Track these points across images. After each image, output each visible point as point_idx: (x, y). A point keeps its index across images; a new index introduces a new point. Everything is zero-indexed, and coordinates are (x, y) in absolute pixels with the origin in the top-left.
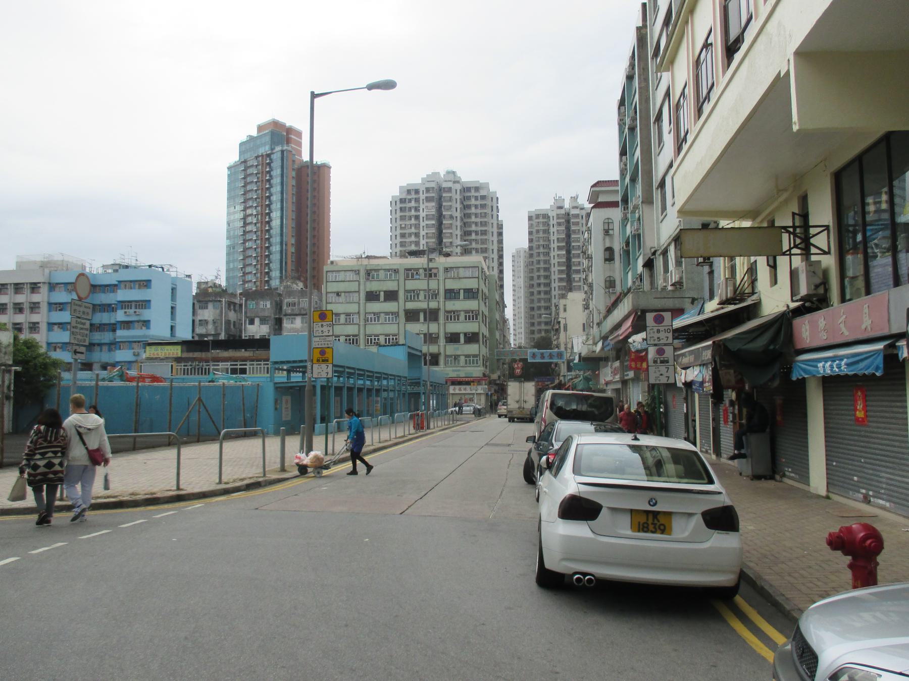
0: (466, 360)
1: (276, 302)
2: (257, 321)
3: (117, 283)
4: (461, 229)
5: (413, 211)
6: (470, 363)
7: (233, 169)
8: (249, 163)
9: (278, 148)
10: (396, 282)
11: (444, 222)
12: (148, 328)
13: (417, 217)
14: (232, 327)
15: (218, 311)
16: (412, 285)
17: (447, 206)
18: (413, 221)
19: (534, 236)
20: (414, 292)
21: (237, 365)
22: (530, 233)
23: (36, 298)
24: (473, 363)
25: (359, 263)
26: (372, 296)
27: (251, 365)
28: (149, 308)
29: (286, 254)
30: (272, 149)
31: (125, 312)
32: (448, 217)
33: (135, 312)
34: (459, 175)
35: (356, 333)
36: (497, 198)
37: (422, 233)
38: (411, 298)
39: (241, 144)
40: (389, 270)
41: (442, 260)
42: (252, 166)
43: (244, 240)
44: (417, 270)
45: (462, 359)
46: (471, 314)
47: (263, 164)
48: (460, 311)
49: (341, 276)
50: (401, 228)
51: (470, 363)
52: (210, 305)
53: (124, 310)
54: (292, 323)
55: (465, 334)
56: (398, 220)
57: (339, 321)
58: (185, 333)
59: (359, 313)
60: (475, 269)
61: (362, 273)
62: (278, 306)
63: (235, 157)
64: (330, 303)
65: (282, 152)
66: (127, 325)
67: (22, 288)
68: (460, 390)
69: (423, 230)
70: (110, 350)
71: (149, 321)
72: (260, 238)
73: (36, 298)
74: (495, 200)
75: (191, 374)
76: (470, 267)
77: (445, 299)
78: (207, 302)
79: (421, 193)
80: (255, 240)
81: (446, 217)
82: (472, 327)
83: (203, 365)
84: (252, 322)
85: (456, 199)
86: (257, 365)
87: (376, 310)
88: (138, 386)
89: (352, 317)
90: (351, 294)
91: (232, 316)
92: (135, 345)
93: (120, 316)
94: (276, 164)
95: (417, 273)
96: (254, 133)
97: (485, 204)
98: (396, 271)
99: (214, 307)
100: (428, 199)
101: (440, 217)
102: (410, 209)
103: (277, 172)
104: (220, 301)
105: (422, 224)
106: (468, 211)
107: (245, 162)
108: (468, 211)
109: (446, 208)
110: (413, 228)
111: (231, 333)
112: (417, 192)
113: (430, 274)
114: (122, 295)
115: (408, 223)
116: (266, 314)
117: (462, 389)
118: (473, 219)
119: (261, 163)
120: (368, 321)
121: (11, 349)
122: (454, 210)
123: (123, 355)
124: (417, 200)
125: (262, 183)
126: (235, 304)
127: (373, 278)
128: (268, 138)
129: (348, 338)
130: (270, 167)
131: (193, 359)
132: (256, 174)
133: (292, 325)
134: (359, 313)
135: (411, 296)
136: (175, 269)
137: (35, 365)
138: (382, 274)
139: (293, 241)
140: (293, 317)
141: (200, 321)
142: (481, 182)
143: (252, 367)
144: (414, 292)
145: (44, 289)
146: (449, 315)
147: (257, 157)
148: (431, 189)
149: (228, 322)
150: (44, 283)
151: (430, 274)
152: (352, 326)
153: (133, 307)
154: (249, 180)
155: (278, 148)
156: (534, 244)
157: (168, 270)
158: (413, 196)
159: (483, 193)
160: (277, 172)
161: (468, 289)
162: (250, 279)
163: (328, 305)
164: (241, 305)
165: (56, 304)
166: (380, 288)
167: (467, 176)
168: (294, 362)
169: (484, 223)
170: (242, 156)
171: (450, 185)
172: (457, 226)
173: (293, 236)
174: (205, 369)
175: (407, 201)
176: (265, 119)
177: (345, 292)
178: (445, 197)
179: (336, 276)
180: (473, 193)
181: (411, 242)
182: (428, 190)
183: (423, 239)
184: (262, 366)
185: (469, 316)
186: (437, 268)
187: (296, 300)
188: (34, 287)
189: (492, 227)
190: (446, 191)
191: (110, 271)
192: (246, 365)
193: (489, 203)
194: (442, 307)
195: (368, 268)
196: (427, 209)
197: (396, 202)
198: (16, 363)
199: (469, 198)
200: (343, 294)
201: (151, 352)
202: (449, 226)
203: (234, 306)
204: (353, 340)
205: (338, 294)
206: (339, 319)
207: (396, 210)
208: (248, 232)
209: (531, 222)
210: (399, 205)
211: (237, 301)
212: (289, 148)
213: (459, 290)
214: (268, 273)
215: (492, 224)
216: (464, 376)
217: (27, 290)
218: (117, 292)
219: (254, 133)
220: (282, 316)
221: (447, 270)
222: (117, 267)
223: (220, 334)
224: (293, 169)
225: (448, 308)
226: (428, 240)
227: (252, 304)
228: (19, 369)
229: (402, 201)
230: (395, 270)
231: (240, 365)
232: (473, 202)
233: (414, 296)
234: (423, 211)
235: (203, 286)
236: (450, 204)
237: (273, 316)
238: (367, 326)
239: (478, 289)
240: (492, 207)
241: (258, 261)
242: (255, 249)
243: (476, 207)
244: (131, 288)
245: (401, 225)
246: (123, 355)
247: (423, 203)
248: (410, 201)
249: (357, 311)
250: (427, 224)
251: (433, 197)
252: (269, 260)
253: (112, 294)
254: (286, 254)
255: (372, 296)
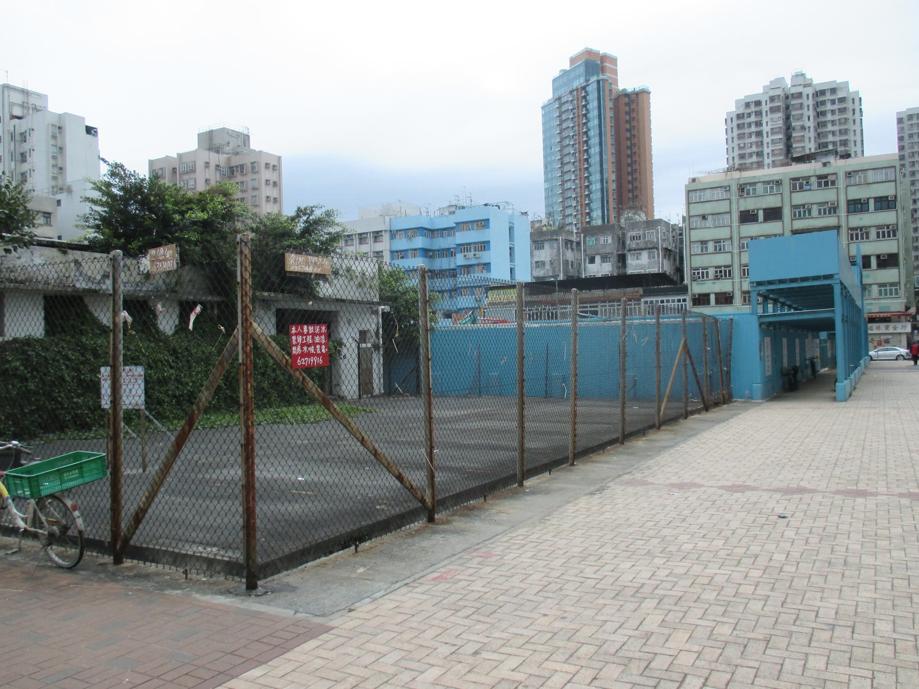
0: (880, 291)
1: (618, 237)
2: (598, 259)
3: (455, 225)
4: (815, 141)
5: (753, 126)
6: (886, 294)
7: (547, 108)
8: (564, 100)
9: (594, 79)
10: (779, 197)
11: (794, 135)
12: (489, 271)
13: (759, 134)
14: (570, 267)
15: (555, 251)
16: (800, 198)
17: (798, 115)
18: (754, 139)
19: (906, 143)
20: (804, 208)
21: (587, 307)
22: (901, 139)
23: (379, 247)
24: (891, 294)
25: (729, 177)
26: (747, 217)
27: (602, 306)
28: (489, 249)
29: (607, 191)
30: (587, 81)
31: (465, 256)
32: (799, 128)
33: (475, 255)
34: (808, 77)
35: (729, 262)
36: (860, 99)
37: (766, 150)
38: (800, 215)
39: (554, 81)
40: (768, 182)
41: (842, 162)
42: (567, 102)
43: (562, 181)
44: (807, 178)
45: (875, 289)
46: (886, 230)
47: (578, 98)
48: (870, 227)
49: (708, 195)
50: (740, 148)
51: (886, 294)
52: (547, 245)
53: (463, 254)
54: (637, 259)
55: (878, 257)
56: (735, 139)
57: (707, 250)
58: (524, 276)
59: (731, 238)
60: (889, 171)
61: (734, 189)
62: (622, 242)
63: (547, 95)
64: (695, 229)
65: (598, 82)
66: (468, 268)
67: (366, 238)
68: (887, 328)
69: (768, 147)
70: (451, 297)
71: (489, 264)
72: (578, 177)
73: (379, 247)
74: (857, 101)
75: (552, 318)
76: (882, 168)
77: (848, 212)
78: (543, 242)
79: (764, 103)
80: (574, 180)
81: (797, 128)
82: (887, 247)
83: (549, 309)
84: (592, 261)
85: (808, 106)
86: (610, 306)
87: (753, 234)
88: (658, 324)
89: (722, 244)
90: (720, 216)
91: (570, 255)
92: (477, 291)
93: (460, 260)
94: (593, 96)
95: (807, 182)
96: (567, 67)
97: (845, 108)
98: (778, 183)
99: (552, 248)
100: (773, 110)
101: (788, 129)
102: (750, 125)
103: (593, 105)
104: (556, 240)
105: (766, 140)
106: (822, 119)
107: (559, 98)
108: (822, 119)
109: (796, 117)
110: (754, 146)
111: (569, 274)
112: (758, 103)
113: (824, 181)
114: (461, 237)
115: (748, 141)
116: (608, 251)
117: (874, 328)
118: (830, 127)
119: (576, 97)
120: (743, 248)
121: (376, 282)
122: (806, 119)
123: (465, 301)
124: (758, 113)
125: (579, 118)
126: (572, 242)
127: (748, 194)
128: (582, 70)
129: (718, 270)
130: (586, 101)
131: (539, 303)
132: (572, 110)
133: (638, 262)
134: (731, 238)
135: (800, 212)
136: (511, 207)
137: (407, 301)
138: (760, 188)
139: (613, 177)
140: (638, 252)
141: (537, 262)
142: (838, 82)
143: (612, 308)
144: (804, 208)
145: (386, 237)
146: (854, 232)
147: (571, 92)
148: (776, 98)
149: (566, 262)
150: (386, 231)
151: (824, 181)
152: (723, 255)
153: (472, 250)
154: (564, 125)
155: (594, 79)
156: (907, 152)
157: (504, 208)
158: (753, 108)
159: (841, 95)
160: (593, 105)
161: (881, 198)
162: (570, 222)
163: (693, 232)
164: (578, 244)
165: (397, 252)
166: (759, 205)
167: (820, 77)
168: (770, 283)
169: (843, 132)
170: (556, 93)
171: (799, 89)
172: (810, 138)
173: (613, 172)
174: (552, 313)
175: (745, 115)
176: (577, 49)
177: (712, 214)
178: (793, 105)
179: (700, 196)
180: (828, 96)
181: (752, 163)
182: (772, 99)
183: (768, 158)
184: (607, 308)
185: (883, 233)
186: (835, 174)
187: (641, 232)
188: (377, 235)
189: (855, 134)
190: (796, 98)
191: (447, 213)
192: (597, 307)
193: (849, 105)
194: (843, 224)
195: (742, 182)
196: (772, 122)
197: (732, 119)
198: (383, 300)
199: (823, 103)
200: (710, 217)
201: (493, 296)
202: (800, 139)
203: (571, 244)
204: (725, 271)
205: (704, 217)
206: (706, 248)
207: (732, 128)
208: (566, 172)
209: (901, 125)
210: (735, 122)
211: (574, 238)
212: (604, 77)
213: (868, 199)
214: (588, 214)
215: (855, 131)
216: (877, 311)
217: (370, 240)
218: (454, 235)
219: (567, 67)
220: (626, 252)
221: (849, 174)
222: (453, 209)
223: (558, 276)
224: (610, 100)
225: (851, 225)
226: (774, 159)
227: (591, 241)
228: (387, 308)
229: (740, 116)
230: (777, 182)
231: (590, 307)
232: (829, 107)
233: (804, 212)
234: (767, 125)
235: (537, 225)
236: (801, 112)
237: (615, 252)
238: (742, 254)
239: (896, 196)
240: (854, 110)
241: (578, 202)
242: (574, 189)
243: (833, 112)
244: (469, 230)
245: (739, 145)
246: (465, 301)
247: (767, 115)
248: (749, 115)
249: (729, 236)
250: (772, 140)
251: (780, 106)
252: (590, 199)
253: (450, 238)
254: (607, 191)
255: (747, 217)
